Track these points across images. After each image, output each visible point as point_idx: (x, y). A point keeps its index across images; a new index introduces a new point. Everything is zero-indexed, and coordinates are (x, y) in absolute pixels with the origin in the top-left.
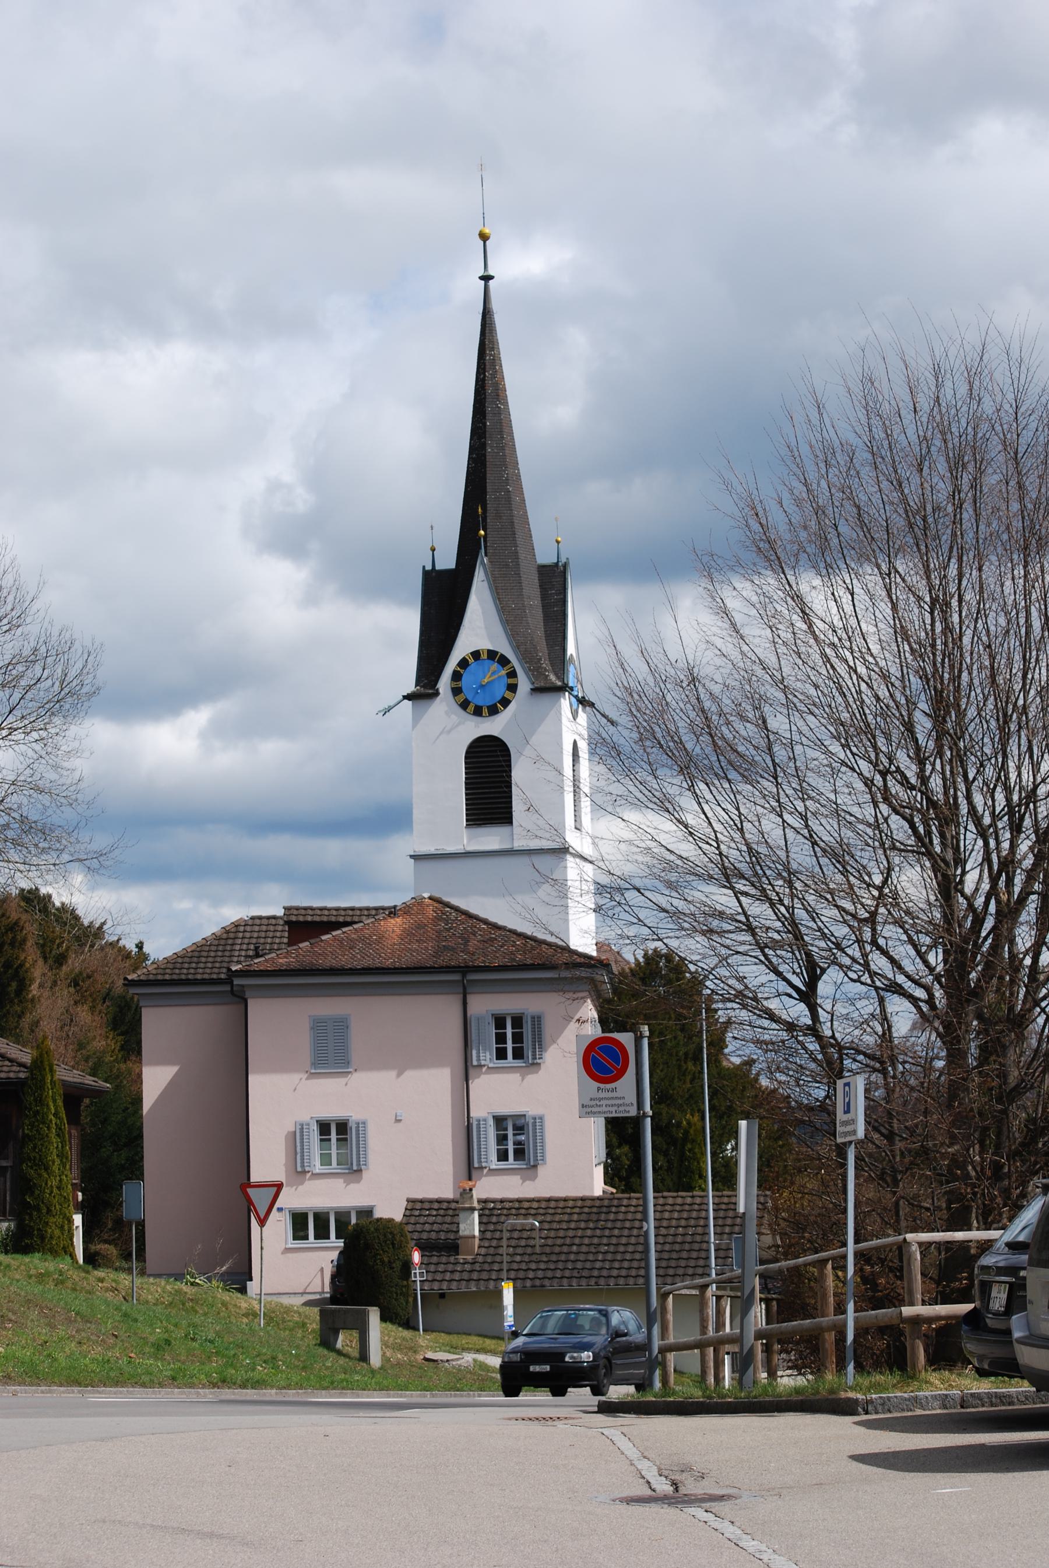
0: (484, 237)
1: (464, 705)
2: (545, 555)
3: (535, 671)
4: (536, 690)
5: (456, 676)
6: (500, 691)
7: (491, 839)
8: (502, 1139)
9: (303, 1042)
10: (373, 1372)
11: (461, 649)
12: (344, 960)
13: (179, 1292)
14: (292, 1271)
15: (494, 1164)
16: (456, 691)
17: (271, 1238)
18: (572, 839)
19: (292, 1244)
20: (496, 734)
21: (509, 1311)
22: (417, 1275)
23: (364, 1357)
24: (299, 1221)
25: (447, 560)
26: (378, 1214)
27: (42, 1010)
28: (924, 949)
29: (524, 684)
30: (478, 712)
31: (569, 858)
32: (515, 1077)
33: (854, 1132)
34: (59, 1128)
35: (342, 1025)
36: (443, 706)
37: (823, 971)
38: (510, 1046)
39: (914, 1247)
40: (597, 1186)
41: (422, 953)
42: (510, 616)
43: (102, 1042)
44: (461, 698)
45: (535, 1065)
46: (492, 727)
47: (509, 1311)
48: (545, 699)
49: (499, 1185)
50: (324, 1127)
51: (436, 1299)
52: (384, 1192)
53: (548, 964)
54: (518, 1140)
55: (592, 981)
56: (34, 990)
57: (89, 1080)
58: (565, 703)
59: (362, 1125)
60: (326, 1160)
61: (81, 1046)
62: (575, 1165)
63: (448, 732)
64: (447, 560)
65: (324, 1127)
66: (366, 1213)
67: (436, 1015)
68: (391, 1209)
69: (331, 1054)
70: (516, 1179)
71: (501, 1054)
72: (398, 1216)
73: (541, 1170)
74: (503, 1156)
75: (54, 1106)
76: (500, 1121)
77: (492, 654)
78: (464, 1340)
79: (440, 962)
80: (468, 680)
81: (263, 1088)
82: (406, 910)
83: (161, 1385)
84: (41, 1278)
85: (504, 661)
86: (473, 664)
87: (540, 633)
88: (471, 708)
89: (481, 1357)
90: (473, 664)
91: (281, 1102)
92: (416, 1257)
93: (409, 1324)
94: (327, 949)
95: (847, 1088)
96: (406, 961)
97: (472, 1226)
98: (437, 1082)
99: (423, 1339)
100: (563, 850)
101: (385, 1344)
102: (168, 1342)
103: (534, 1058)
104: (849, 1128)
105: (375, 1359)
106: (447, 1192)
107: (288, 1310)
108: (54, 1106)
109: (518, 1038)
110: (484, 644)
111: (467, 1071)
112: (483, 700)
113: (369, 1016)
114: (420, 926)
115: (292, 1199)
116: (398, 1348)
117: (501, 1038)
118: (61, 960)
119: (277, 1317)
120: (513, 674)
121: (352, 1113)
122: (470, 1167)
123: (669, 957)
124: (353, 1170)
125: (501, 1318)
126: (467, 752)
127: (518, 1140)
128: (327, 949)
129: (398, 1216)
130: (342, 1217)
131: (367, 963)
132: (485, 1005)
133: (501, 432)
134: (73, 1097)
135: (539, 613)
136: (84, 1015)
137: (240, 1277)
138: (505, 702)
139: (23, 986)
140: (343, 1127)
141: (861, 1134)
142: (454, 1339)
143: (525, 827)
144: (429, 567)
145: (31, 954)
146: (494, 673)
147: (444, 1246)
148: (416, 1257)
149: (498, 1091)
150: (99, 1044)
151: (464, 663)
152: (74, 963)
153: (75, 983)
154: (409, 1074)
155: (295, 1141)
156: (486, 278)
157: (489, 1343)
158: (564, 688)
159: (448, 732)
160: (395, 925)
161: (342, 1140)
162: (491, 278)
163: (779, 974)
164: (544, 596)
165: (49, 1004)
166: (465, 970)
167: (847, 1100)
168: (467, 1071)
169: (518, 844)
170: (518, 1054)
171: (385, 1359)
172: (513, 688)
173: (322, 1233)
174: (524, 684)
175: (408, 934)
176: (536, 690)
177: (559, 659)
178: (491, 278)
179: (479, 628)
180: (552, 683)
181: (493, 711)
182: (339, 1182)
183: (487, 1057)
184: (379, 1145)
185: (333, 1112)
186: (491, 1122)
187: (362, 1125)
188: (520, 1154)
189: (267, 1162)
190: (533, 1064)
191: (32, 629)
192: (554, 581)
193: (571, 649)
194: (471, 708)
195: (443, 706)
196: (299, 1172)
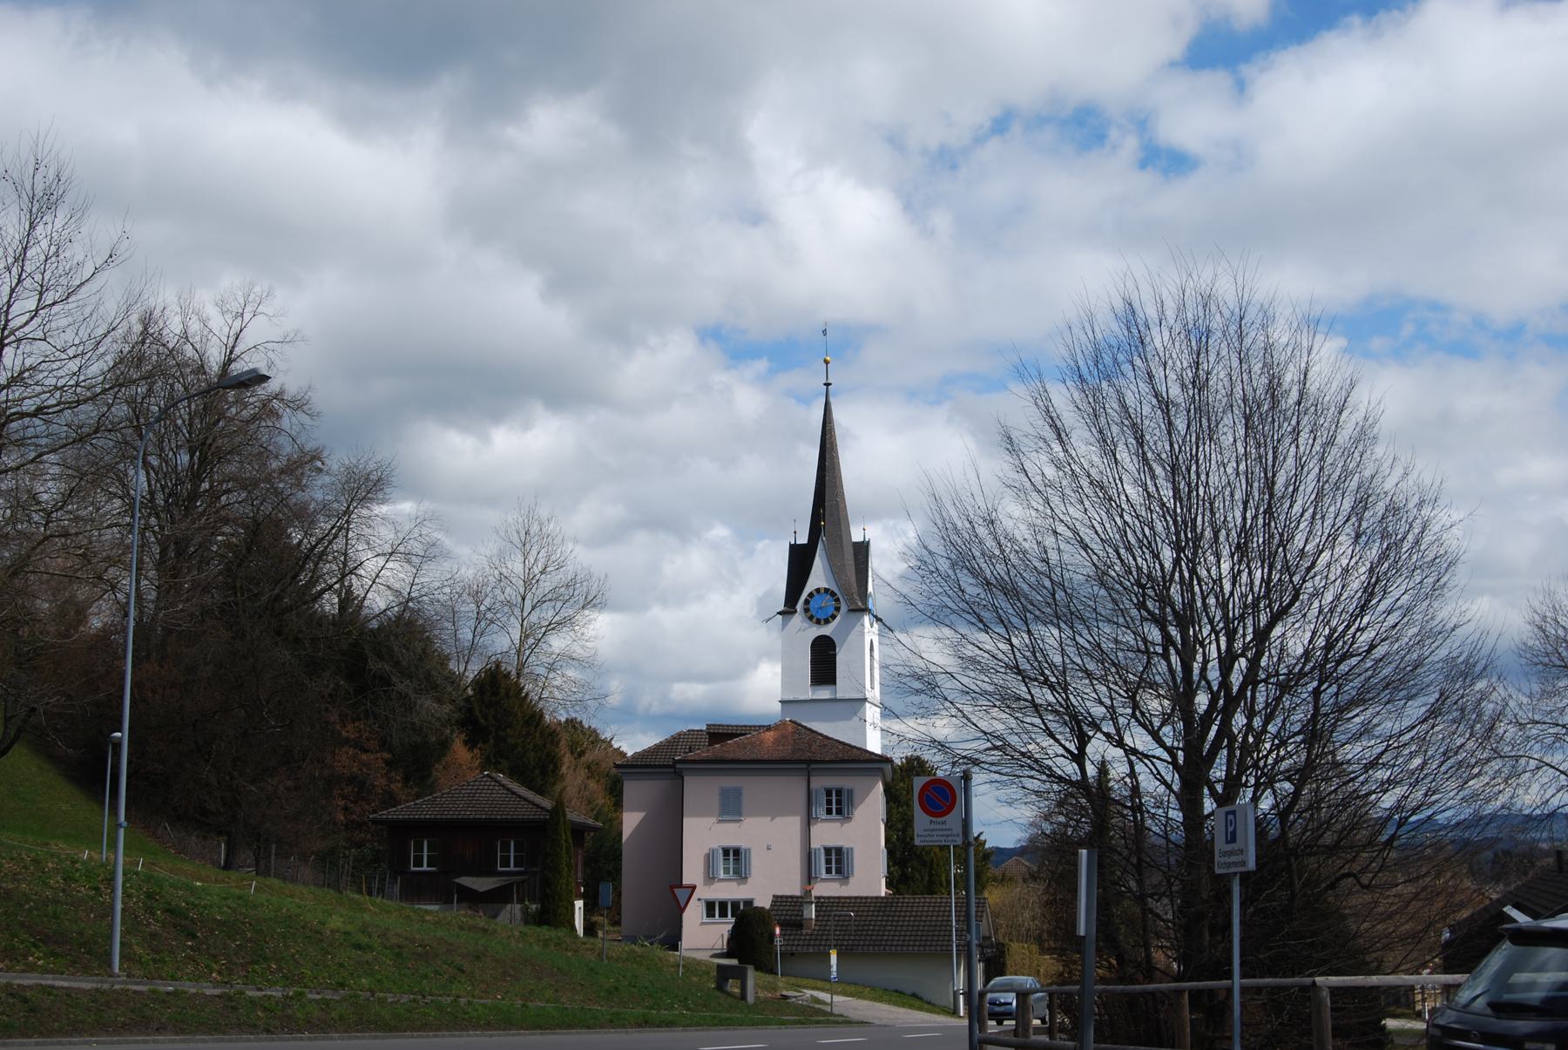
1: (811, 618)
3: (850, 600)
5: (807, 602)
6: (831, 611)
7: (824, 693)
8: (828, 861)
9: (715, 802)
10: (748, 1007)
11: (810, 587)
12: (740, 755)
13: (633, 951)
14: (703, 936)
15: (824, 875)
16: (806, 610)
17: (693, 915)
18: (868, 695)
19: (706, 920)
21: (834, 968)
22: (778, 941)
23: (743, 996)
24: (710, 906)
25: (803, 539)
26: (756, 904)
27: (568, 780)
28: (1157, 722)
29: (844, 608)
30: (818, 622)
32: (838, 825)
33: (1243, 863)
34: (568, 849)
35: (738, 792)
36: (798, 619)
37: (1090, 738)
39: (1325, 993)
40: (883, 891)
41: (784, 752)
42: (835, 569)
43: (602, 800)
45: (849, 819)
46: (826, 630)
47: (834, 968)
48: (853, 615)
49: (826, 888)
50: (726, 852)
51: (788, 956)
52: (760, 890)
53: (859, 761)
54: (838, 860)
55: (882, 770)
56: (564, 769)
57: (590, 821)
58: (867, 619)
59: (748, 851)
60: (726, 871)
61: (589, 802)
62: (870, 877)
63: (804, 633)
64: (803, 539)
65: (726, 852)
66: (749, 903)
67: (792, 788)
68: (763, 901)
69: (731, 808)
70: (836, 885)
71: (829, 812)
72: (768, 906)
73: (852, 880)
74: (829, 871)
75: (565, 836)
76: (828, 851)
77: (826, 590)
78: (805, 982)
79: (795, 757)
80: (813, 604)
81: (689, 824)
82: (776, 727)
83: (602, 1027)
84: (546, 943)
85: (833, 594)
86: (816, 596)
87: (853, 579)
89: (815, 993)
90: (816, 596)
91: (702, 835)
92: (778, 931)
93: (773, 972)
94: (730, 748)
95: (1231, 817)
96: (775, 756)
97: (812, 912)
98: (794, 823)
99: (781, 981)
100: (865, 700)
101: (756, 985)
102: (617, 989)
104: (1239, 858)
105: (750, 999)
106: (796, 891)
107: (699, 963)
108: (565, 836)
109: (839, 802)
110: (823, 584)
111: (809, 820)
112: (822, 616)
113: (753, 787)
114: (784, 736)
115: (705, 892)
116: (765, 988)
117: (829, 802)
118: (582, 754)
119: (692, 966)
120: (837, 600)
121: (742, 843)
122: (809, 877)
123: (918, 758)
124: (741, 874)
125: (830, 973)
127: (838, 860)
128: (730, 748)
129: (768, 906)
130: (735, 904)
131: (754, 757)
132: (820, 783)
134: (579, 831)
135: (852, 562)
136: (592, 785)
137: (673, 942)
138: (834, 617)
139: (556, 768)
140: (737, 852)
141: (1251, 864)
142: (799, 981)
143: (843, 688)
145: (563, 749)
146: (827, 602)
147: (794, 924)
148: (778, 931)
149: (827, 833)
150: (601, 801)
151: (811, 595)
152: (589, 757)
153: (589, 768)
154: (778, 819)
155: (709, 859)
156: (827, 385)
157: (820, 984)
158: (866, 610)
159: (804, 633)
160: (770, 735)
161: (737, 860)
163: (1057, 740)
164: (856, 560)
165: (573, 780)
166: (809, 762)
167: (1231, 829)
168: (809, 820)
169: (839, 696)
170: (839, 812)
171: (757, 998)
172: (838, 609)
173: (723, 914)
174: (844, 608)
175: (777, 741)
177: (864, 594)
179: (818, 577)
180: (860, 606)
181: (827, 622)
182: (734, 884)
183: (822, 814)
184: (757, 863)
185: (731, 843)
187: (748, 851)
188: (839, 871)
189: (692, 871)
191: (570, 569)
193: (870, 589)
195: (798, 619)
196: (710, 878)
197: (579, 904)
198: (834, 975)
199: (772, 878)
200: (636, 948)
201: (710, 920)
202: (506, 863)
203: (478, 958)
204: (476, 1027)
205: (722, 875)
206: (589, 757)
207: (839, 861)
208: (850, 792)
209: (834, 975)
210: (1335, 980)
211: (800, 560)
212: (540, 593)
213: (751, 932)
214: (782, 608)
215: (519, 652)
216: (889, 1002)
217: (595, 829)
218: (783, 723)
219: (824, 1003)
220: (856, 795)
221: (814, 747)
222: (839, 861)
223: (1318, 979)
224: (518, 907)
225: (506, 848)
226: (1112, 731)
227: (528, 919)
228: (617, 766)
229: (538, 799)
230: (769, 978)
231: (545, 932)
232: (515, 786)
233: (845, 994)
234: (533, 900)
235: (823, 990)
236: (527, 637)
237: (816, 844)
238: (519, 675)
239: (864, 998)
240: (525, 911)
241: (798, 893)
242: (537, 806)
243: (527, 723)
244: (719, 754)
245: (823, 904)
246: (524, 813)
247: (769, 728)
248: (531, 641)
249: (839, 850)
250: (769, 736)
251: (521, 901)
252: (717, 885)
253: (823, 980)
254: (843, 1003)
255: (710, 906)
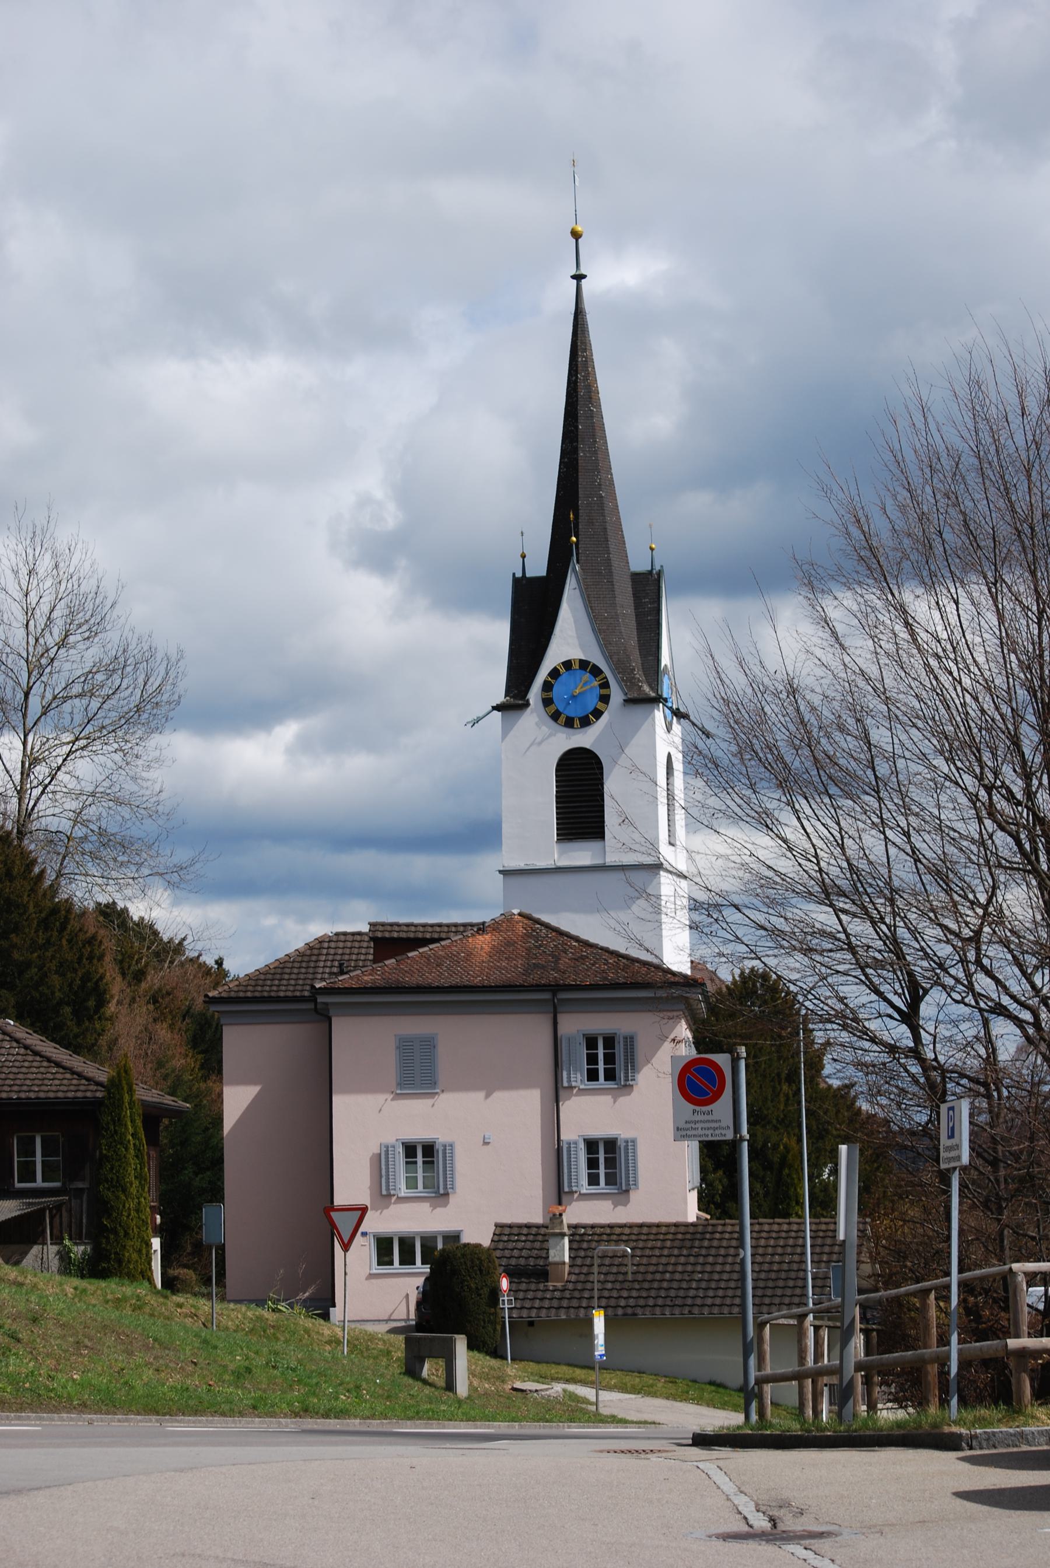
0: (576, 235)
1: (555, 716)
2: (638, 563)
3: (628, 681)
4: (629, 701)
5: (547, 686)
6: (592, 702)
7: (582, 854)
8: (592, 1164)
10: (460, 1402)
11: (552, 659)
12: (431, 978)
13: (260, 1318)
14: (375, 1297)
15: (585, 1188)
16: (547, 702)
17: (354, 1263)
18: (666, 852)
19: (376, 1269)
20: (588, 747)
22: (506, 1302)
23: (450, 1385)
24: (384, 1247)
25: (538, 568)
26: (465, 1239)
29: (617, 695)
30: (569, 723)
31: (662, 873)
32: (607, 1099)
33: (959, 1158)
35: (429, 1044)
36: (533, 719)
37: (926, 992)
38: (601, 1066)
40: (691, 1212)
41: (511, 970)
42: (601, 624)
43: (182, 1060)
44: (552, 709)
46: (584, 739)
48: (639, 710)
49: (581, 1212)
50: (410, 1150)
51: (524, 1327)
52: (473, 1214)
53: (641, 983)
54: (608, 1160)
56: (112, 1007)
57: (168, 1100)
58: (659, 715)
60: (411, 1183)
61: (160, 1065)
62: (668, 1190)
63: (538, 746)
64: (538, 568)
65: (410, 1150)
66: (453, 1238)
67: (526, 1034)
69: (417, 1075)
70: (606, 1205)
71: (593, 1076)
72: (486, 1242)
74: (593, 1180)
75: (132, 1127)
76: (591, 1145)
77: (584, 664)
78: (553, 1370)
79: (533, 978)
80: (559, 691)
81: (347, 1108)
82: (495, 926)
83: (241, 1414)
84: (118, 1303)
85: (596, 671)
86: (565, 675)
87: (633, 642)
88: (562, 719)
90: (565, 675)
91: (366, 1124)
92: (504, 1284)
94: (414, 966)
95: (951, 1112)
96: (496, 978)
97: (562, 1252)
98: (526, 1104)
99: (511, 1369)
101: (472, 1373)
103: (627, 1080)
104: (953, 1154)
105: (462, 1388)
107: (372, 1337)
108: (132, 1127)
109: (610, 1059)
110: (576, 654)
111: (557, 1093)
113: (455, 1035)
114: (509, 943)
115: (376, 1223)
116: (485, 1377)
117: (592, 1059)
118: (139, 976)
119: (361, 1345)
120: (605, 685)
122: (560, 1192)
124: (439, 1193)
125: (592, 1346)
126: (558, 765)
127: (608, 1160)
128: (414, 966)
129: (486, 1242)
130: (428, 1242)
131: (455, 980)
132: (575, 1025)
133: (594, 436)
136: (163, 1032)
137: (323, 1303)
138: (598, 714)
139: (102, 1003)
140: (429, 1149)
141: (965, 1159)
143: (617, 845)
144: (519, 575)
146: (584, 684)
147: (533, 1273)
148: (504, 1284)
149: (589, 1114)
150: (178, 1063)
151: (555, 673)
153: (154, 1000)
154: (498, 1095)
155: (380, 1163)
156: (579, 277)
157: (579, 1373)
158: (658, 699)
160: (483, 942)
162: (584, 277)
164: (638, 604)
165: (127, 1021)
166: (555, 988)
168: (557, 1093)
169: (611, 859)
170: (610, 1076)
171: (472, 1388)
172: (605, 699)
174: (617, 695)
175: (497, 952)
176: (629, 701)
177: (653, 669)
178: (584, 277)
179: (570, 639)
181: (585, 722)
182: (426, 1206)
183: (578, 1078)
184: (466, 1168)
185: (419, 1134)
186: (582, 1145)
188: (611, 1180)
189: (351, 1185)
190: (625, 1086)
191: (112, 638)
192: (648, 589)
193: (665, 660)
194: (562, 719)
195: (533, 719)
196: (384, 1196)
197: (156, 1243)
198: (600, 1349)
199: (492, 1193)
200: (266, 1314)
201: (385, 1270)
202: (28, 1174)
203: (35, 1320)
204: (70, 1408)
205: (403, 1191)
206: (154, 980)
207: (611, 1163)
208: (630, 1041)
209: (600, 1349)
210: (1032, 1266)
211: (533, 610)
212: (58, 682)
213: (459, 1294)
214: (500, 697)
215: (21, 793)
216: (699, 1401)
217: (177, 1113)
218: (507, 919)
219: (586, 1401)
220: (641, 1048)
221: (564, 961)
222: (611, 1163)
223: (1015, 1266)
224: (53, 1249)
225: (27, 1150)
226: (961, 975)
227: (67, 1266)
228: (210, 1001)
229: (77, 1062)
230: (494, 1363)
231: (113, 1287)
232: (35, 1040)
233: (623, 1389)
234: (77, 1239)
235: (584, 1383)
236: (35, 761)
237: (568, 1134)
238: (21, 834)
239: (654, 1395)
240: (64, 1257)
241: (538, 1219)
242: (80, 1076)
243: (45, 924)
244: (394, 977)
245: (584, 1237)
246: (55, 1087)
247: (481, 928)
248: (41, 771)
249: (611, 1144)
250: (483, 942)
251: (57, 1240)
252: (395, 1209)
253: (583, 1364)
254: (612, 1401)
255: (384, 1247)
